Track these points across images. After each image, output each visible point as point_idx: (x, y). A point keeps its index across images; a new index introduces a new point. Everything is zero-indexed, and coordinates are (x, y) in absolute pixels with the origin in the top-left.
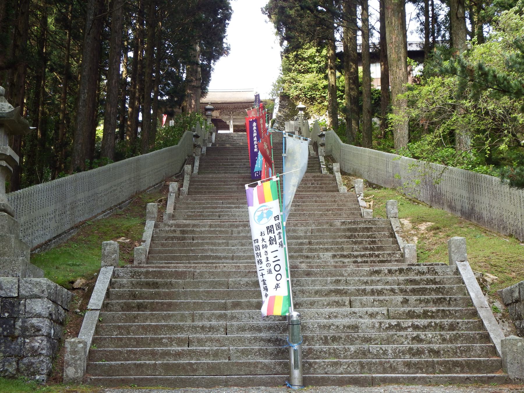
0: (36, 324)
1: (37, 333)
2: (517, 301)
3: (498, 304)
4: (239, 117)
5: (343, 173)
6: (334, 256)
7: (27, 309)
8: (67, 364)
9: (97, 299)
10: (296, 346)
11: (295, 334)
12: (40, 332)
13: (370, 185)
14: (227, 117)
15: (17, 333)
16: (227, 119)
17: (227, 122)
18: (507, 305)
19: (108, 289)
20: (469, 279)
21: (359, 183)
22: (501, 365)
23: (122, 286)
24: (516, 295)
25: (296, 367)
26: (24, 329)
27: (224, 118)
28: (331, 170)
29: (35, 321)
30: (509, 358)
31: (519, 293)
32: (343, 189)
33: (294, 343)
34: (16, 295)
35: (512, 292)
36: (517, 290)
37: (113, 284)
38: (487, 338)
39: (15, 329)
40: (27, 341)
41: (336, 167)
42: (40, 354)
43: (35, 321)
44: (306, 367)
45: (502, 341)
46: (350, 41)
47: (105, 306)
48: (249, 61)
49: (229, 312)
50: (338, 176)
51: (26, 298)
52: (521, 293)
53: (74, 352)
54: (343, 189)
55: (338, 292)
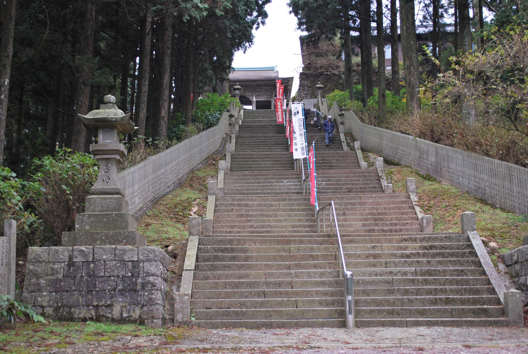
0: (152, 281)
1: (154, 288)
2: (516, 263)
3: (501, 266)
4: (261, 94)
5: (363, 150)
6: (364, 225)
7: (145, 270)
8: (177, 311)
9: (190, 262)
10: (350, 298)
11: (349, 288)
12: (156, 287)
13: (387, 162)
14: (250, 94)
15: (139, 287)
16: (250, 96)
17: (251, 98)
18: (508, 266)
19: (197, 255)
20: (477, 245)
21: (379, 161)
22: (503, 312)
23: (207, 251)
24: (515, 258)
25: (350, 313)
26: (143, 286)
27: (248, 94)
28: (353, 149)
29: (151, 279)
30: (510, 306)
31: (518, 256)
32: (364, 164)
33: (349, 295)
34: (136, 259)
35: (511, 255)
36: (516, 254)
37: (200, 249)
38: (493, 291)
39: (137, 284)
40: (146, 294)
41: (357, 145)
42: (157, 303)
43: (151, 279)
44: (357, 314)
45: (504, 293)
46: (364, 29)
47: (197, 267)
48: (275, 46)
49: (292, 271)
50: (359, 153)
51: (144, 262)
52: (519, 257)
53: (183, 303)
54: (364, 164)
55: (375, 256)
